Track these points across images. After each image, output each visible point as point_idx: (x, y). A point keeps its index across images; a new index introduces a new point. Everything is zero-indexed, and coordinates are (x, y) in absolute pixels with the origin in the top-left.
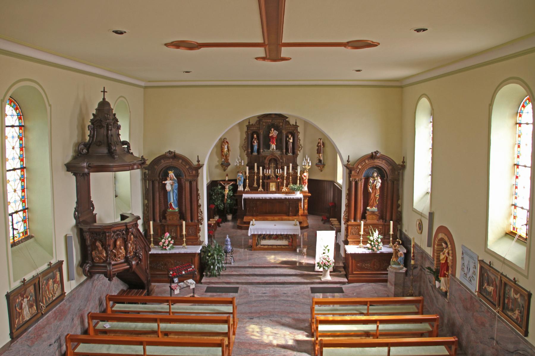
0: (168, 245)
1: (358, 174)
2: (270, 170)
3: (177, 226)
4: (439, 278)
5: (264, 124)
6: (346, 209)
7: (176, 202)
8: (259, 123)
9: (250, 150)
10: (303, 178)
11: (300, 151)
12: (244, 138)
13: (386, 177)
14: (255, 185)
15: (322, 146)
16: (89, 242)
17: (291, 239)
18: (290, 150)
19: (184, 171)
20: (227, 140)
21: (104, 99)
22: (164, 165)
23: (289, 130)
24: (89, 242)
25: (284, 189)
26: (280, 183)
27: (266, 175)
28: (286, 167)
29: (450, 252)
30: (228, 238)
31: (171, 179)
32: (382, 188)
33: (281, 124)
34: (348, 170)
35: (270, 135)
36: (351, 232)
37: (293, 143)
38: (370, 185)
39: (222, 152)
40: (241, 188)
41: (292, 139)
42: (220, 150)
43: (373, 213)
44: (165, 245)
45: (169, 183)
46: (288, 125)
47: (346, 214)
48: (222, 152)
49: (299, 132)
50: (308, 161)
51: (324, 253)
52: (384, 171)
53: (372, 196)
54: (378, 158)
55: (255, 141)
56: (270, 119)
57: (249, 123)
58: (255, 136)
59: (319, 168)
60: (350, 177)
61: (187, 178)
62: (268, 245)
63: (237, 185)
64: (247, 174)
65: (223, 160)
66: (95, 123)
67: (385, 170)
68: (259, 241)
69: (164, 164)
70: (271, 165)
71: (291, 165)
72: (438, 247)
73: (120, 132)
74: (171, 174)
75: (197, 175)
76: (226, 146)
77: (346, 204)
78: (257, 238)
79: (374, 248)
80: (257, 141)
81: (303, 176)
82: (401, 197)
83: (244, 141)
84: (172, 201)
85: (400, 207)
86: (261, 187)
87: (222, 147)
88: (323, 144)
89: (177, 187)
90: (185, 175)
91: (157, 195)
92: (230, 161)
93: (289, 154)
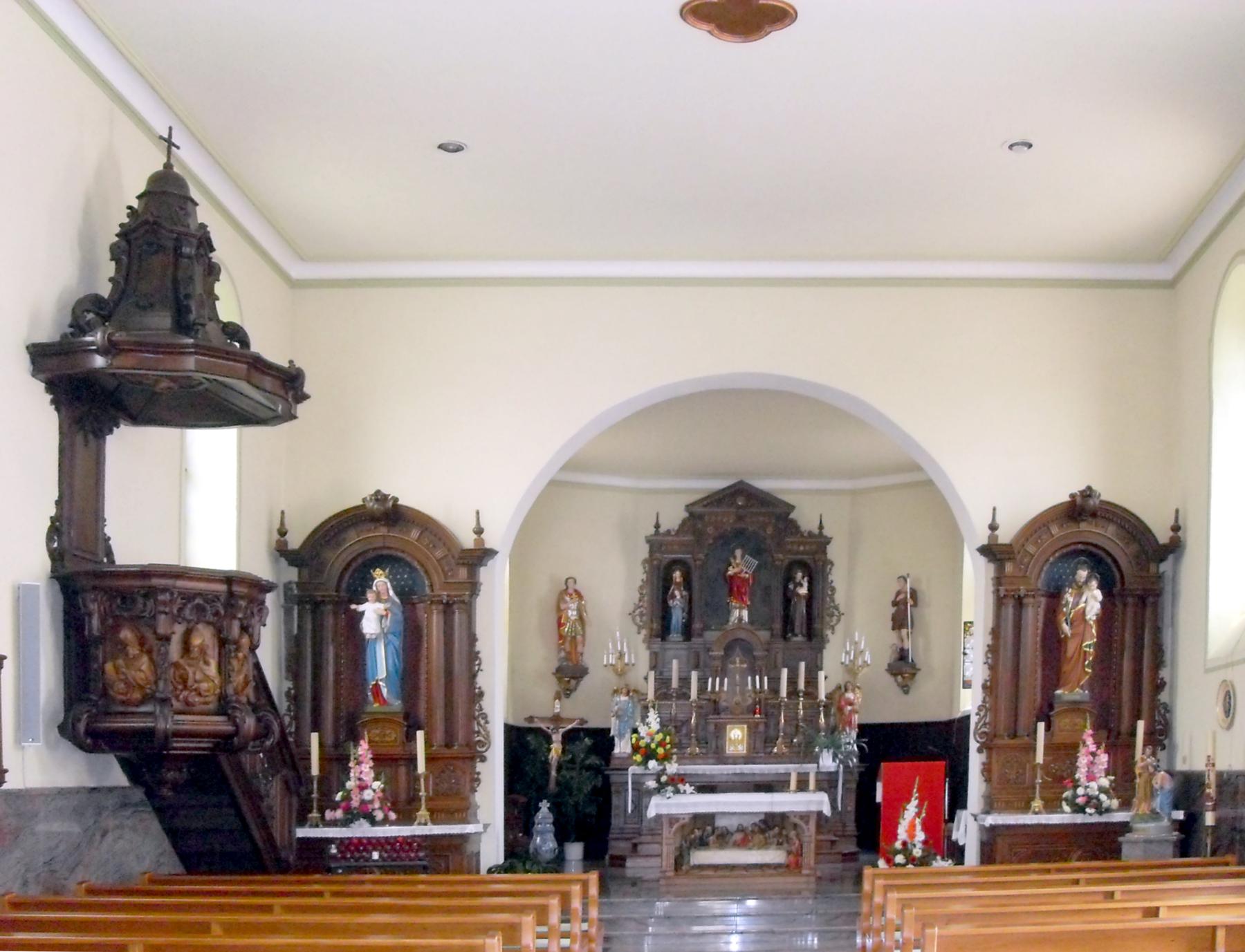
2: (726, 680)
6: (984, 701)
7: (396, 680)
11: (833, 628)
12: (640, 583)
15: (910, 602)
16: (95, 622)
17: (797, 842)
18: (797, 623)
19: (426, 572)
20: (578, 587)
22: (358, 548)
23: (798, 553)
24: (95, 622)
26: (762, 728)
28: (785, 673)
32: (1106, 619)
34: (992, 567)
37: (810, 599)
38: (1065, 614)
39: (560, 625)
41: (806, 584)
43: (1075, 707)
45: (375, 611)
47: (985, 716)
52: (1115, 569)
53: (1071, 647)
54: (1094, 515)
55: (677, 593)
57: (657, 526)
59: (899, 678)
61: (437, 592)
63: (613, 739)
67: (1115, 561)
69: (355, 541)
71: (802, 665)
73: (219, 288)
74: (380, 579)
75: (473, 587)
76: (574, 606)
77: (986, 681)
80: (684, 593)
82: (1168, 657)
83: (638, 596)
85: (1167, 688)
87: (559, 610)
88: (914, 594)
90: (431, 586)
91: (330, 653)
92: (588, 660)
93: (795, 639)
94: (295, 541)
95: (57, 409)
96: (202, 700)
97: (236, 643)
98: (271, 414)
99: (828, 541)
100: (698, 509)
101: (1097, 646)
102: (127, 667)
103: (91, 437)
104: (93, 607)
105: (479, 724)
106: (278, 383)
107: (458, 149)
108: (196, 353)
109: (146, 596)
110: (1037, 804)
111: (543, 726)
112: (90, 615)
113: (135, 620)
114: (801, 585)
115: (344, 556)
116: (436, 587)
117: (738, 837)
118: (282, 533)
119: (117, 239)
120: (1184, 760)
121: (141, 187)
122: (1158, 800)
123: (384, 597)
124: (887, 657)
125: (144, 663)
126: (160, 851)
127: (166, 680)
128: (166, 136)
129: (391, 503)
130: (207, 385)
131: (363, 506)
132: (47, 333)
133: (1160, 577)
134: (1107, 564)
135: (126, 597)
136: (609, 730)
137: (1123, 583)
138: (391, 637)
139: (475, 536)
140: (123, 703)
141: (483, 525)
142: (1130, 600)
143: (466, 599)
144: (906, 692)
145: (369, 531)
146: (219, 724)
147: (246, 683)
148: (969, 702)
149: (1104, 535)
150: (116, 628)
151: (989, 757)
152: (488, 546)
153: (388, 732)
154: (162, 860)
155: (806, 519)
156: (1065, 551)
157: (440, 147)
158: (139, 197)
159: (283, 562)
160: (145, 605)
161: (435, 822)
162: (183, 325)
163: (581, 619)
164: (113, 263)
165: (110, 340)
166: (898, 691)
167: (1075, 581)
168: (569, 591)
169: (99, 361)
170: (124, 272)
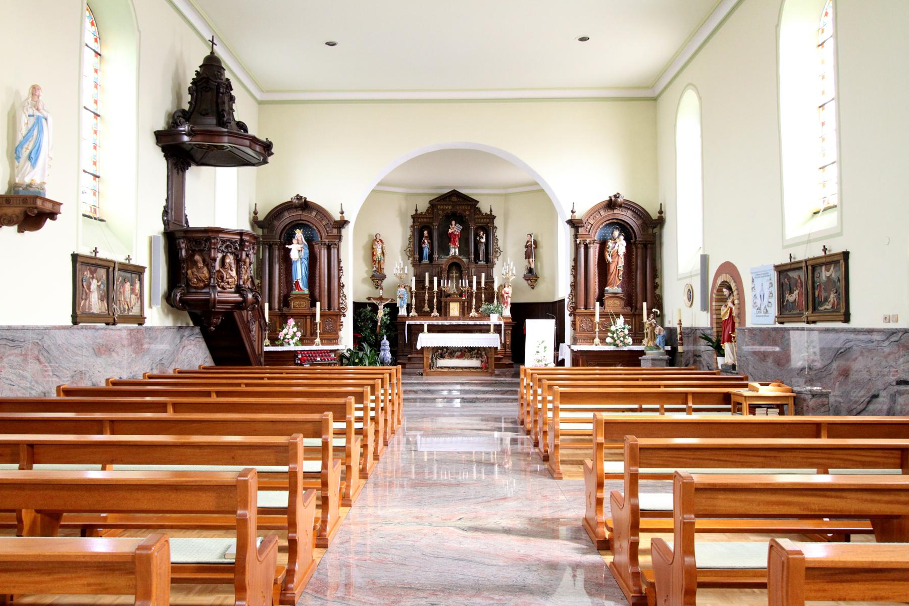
0: (292, 338)
1: (589, 232)
3: (306, 316)
4: (721, 346)
5: (440, 212)
7: (305, 279)
8: (433, 210)
9: (417, 256)
10: (502, 296)
13: (634, 238)
14: (427, 309)
15: (533, 246)
19: (319, 231)
21: (212, 53)
22: (288, 221)
25: (473, 313)
26: (466, 303)
27: (443, 289)
28: (475, 279)
29: (736, 302)
30: (385, 339)
31: (298, 243)
32: (628, 255)
33: (467, 213)
34: (573, 230)
35: (450, 231)
36: (580, 326)
37: (487, 244)
38: (608, 252)
39: (373, 255)
40: (403, 312)
41: (484, 237)
42: (370, 253)
43: (615, 295)
44: (288, 336)
46: (478, 214)
47: (572, 299)
48: (373, 255)
49: (496, 228)
50: (511, 267)
51: (538, 352)
53: (612, 268)
54: (620, 206)
55: (426, 241)
56: (449, 205)
57: (416, 210)
58: (426, 232)
60: (576, 236)
62: (449, 367)
64: (414, 289)
65: (375, 269)
66: (199, 84)
68: (434, 361)
69: (287, 217)
70: (451, 275)
71: (483, 275)
72: (717, 304)
74: (299, 234)
75: (340, 237)
76: (380, 247)
78: (430, 357)
79: (618, 342)
81: (503, 293)
84: (299, 276)
85: (659, 287)
86: (435, 310)
88: (535, 242)
89: (307, 256)
90: (321, 237)
92: (385, 272)
93: (480, 263)
94: (261, 217)
95: (167, 159)
96: (229, 286)
97: (245, 262)
98: (257, 161)
99: (494, 217)
100: (434, 202)
101: (624, 267)
102: (198, 272)
103: (180, 171)
104: (183, 245)
105: (342, 299)
106: (262, 148)
107: (328, 44)
108: (228, 135)
109: (206, 241)
110: (597, 340)
111: (374, 302)
112: (181, 249)
113: (201, 252)
114: (483, 238)
115: (282, 224)
116: (324, 237)
117: (458, 354)
118: (256, 213)
119: (191, 85)
120: (669, 322)
121: (201, 63)
122: (658, 340)
123: (300, 242)
124: (524, 272)
125: (205, 270)
126: (206, 356)
127: (214, 278)
128: (211, 40)
129: (303, 200)
130: (230, 148)
131: (291, 201)
132: (161, 125)
133: (654, 235)
134: (627, 228)
135: (197, 241)
136: (396, 304)
137: (636, 238)
138: (303, 260)
139: (341, 215)
140: (195, 288)
141: (344, 210)
142: (639, 246)
143: (337, 243)
144: (533, 288)
145: (294, 212)
146: (236, 297)
147: (248, 279)
148: (563, 291)
149: (626, 216)
150: (193, 256)
151: (575, 318)
152: (346, 219)
153: (302, 303)
154: (206, 360)
155: (484, 208)
156: (607, 222)
157: (327, 44)
158: (200, 67)
159: (256, 226)
160: (205, 245)
161: (322, 344)
162: (221, 123)
163: (383, 253)
164: (190, 96)
165: (191, 130)
166: (529, 288)
167: (613, 237)
168: (376, 240)
169: (186, 139)
170: (194, 100)
